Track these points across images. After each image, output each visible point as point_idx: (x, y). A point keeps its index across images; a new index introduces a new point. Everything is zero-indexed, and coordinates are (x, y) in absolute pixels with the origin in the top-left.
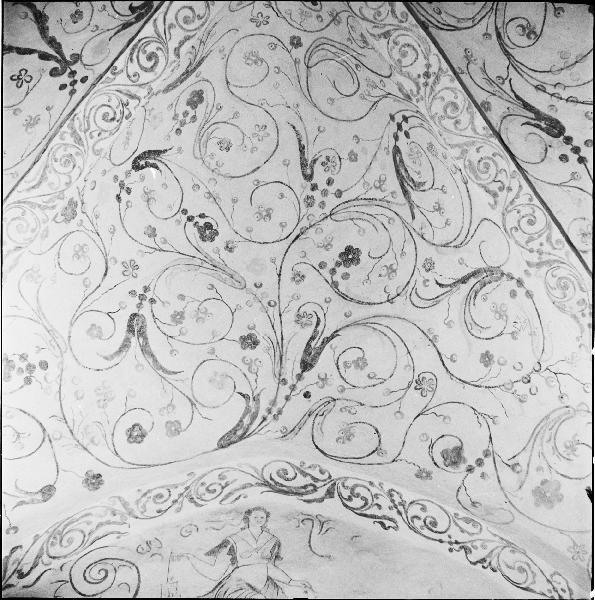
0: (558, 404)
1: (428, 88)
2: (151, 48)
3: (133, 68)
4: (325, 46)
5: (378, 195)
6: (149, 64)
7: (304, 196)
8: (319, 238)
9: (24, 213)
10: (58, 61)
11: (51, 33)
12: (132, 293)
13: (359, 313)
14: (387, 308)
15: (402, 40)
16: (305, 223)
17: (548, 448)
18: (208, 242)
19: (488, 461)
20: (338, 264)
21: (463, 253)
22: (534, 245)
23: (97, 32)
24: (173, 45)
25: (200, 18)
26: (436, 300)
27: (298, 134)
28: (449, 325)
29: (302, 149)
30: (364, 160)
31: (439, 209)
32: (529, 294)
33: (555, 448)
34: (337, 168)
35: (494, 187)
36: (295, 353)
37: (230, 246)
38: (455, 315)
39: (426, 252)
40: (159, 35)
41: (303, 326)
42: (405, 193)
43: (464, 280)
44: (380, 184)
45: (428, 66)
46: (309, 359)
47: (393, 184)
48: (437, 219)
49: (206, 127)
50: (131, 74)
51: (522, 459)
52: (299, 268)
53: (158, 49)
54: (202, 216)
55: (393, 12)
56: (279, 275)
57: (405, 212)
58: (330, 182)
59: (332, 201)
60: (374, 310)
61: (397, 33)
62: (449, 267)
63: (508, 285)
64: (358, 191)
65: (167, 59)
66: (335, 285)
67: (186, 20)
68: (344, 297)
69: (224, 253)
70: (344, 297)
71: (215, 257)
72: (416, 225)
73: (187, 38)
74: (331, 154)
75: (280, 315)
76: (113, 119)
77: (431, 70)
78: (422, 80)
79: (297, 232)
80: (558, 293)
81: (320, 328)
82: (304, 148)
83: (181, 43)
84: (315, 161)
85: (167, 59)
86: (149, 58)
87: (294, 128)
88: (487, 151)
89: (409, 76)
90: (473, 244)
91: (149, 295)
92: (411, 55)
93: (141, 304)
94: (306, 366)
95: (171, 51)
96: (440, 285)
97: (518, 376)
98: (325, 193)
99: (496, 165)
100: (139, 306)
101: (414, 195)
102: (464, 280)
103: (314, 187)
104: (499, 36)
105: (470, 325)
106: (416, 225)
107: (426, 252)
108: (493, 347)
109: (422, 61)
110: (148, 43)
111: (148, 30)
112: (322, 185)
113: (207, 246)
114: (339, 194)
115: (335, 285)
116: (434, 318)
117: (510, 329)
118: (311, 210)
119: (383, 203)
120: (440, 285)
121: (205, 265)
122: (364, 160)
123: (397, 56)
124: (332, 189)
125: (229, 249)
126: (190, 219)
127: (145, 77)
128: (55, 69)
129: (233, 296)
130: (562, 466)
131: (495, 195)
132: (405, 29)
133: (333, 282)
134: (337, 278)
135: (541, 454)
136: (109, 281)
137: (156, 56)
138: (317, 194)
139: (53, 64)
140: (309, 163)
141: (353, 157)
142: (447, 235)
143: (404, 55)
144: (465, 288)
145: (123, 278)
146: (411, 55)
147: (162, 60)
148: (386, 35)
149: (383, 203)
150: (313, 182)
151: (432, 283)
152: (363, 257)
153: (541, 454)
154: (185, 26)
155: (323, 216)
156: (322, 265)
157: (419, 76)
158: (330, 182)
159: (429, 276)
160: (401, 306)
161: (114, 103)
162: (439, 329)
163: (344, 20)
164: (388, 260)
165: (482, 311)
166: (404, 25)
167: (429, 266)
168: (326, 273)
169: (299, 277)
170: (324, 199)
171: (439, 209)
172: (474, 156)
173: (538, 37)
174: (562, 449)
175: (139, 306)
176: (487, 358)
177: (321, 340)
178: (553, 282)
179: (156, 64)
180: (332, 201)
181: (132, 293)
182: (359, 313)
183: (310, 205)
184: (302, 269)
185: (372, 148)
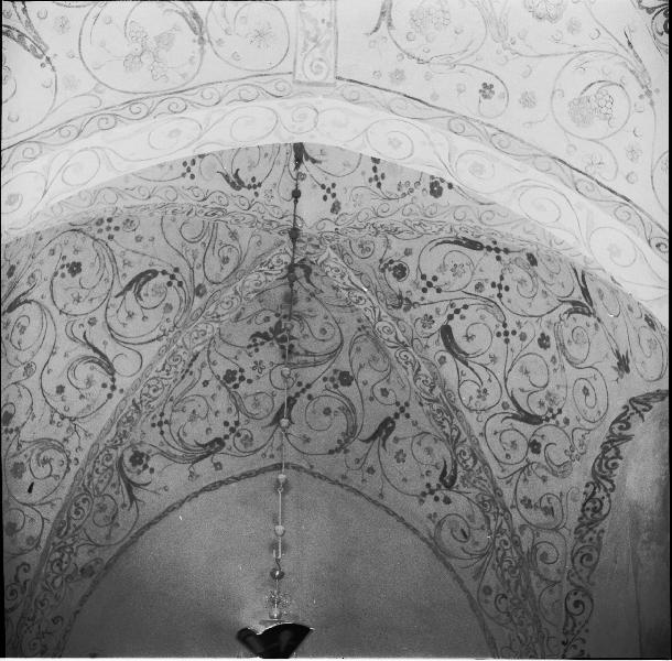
0: (61, 441)
5: (120, 264)
8: (79, 243)
13: (47, 302)
14: (55, 313)
15: (235, 301)
16: (85, 228)
17: (37, 451)
19: (14, 433)
21: (111, 342)
22: (144, 397)
26: (74, 339)
28: (66, 355)
30: (139, 247)
31: (131, 315)
32: (110, 396)
33: (39, 455)
35: (167, 367)
38: (73, 355)
39: (99, 316)
42: (129, 286)
43: (96, 350)
44: (127, 263)
47: (132, 273)
48: (123, 315)
51: (24, 446)
57: (117, 290)
59: (104, 236)
60: (52, 308)
62: (98, 336)
63: (107, 380)
64: (117, 250)
66: (56, 274)
72: (113, 301)
74: (136, 222)
79: (78, 228)
80: (125, 419)
88: (185, 357)
90: (120, 349)
96: (84, 336)
97: (61, 410)
101: (130, 294)
102: (96, 350)
105: (72, 368)
106: (113, 301)
107: (99, 316)
108: (69, 389)
112: (112, 225)
114: (111, 237)
115: (56, 274)
116: (65, 344)
117: (83, 392)
119: (116, 271)
120: (84, 336)
122: (139, 247)
123: (226, 300)
124: (112, 232)
130: (34, 464)
131: (163, 369)
135: (32, 451)
138: (106, 224)
141: (139, 239)
142: (117, 327)
143: (227, 303)
144: (90, 352)
148: (236, 293)
149: (116, 271)
151: (83, 329)
152: (78, 276)
153: (32, 451)
158: (117, 228)
159: (87, 326)
160: (61, 320)
162: (60, 353)
164: (83, 293)
165: (84, 371)
167: (92, 322)
171: (131, 315)
172: (181, 352)
174: (41, 458)
176: (60, 389)
178: (130, 415)
180: (104, 236)
182: (47, 302)
183: (97, 224)
185: (149, 251)
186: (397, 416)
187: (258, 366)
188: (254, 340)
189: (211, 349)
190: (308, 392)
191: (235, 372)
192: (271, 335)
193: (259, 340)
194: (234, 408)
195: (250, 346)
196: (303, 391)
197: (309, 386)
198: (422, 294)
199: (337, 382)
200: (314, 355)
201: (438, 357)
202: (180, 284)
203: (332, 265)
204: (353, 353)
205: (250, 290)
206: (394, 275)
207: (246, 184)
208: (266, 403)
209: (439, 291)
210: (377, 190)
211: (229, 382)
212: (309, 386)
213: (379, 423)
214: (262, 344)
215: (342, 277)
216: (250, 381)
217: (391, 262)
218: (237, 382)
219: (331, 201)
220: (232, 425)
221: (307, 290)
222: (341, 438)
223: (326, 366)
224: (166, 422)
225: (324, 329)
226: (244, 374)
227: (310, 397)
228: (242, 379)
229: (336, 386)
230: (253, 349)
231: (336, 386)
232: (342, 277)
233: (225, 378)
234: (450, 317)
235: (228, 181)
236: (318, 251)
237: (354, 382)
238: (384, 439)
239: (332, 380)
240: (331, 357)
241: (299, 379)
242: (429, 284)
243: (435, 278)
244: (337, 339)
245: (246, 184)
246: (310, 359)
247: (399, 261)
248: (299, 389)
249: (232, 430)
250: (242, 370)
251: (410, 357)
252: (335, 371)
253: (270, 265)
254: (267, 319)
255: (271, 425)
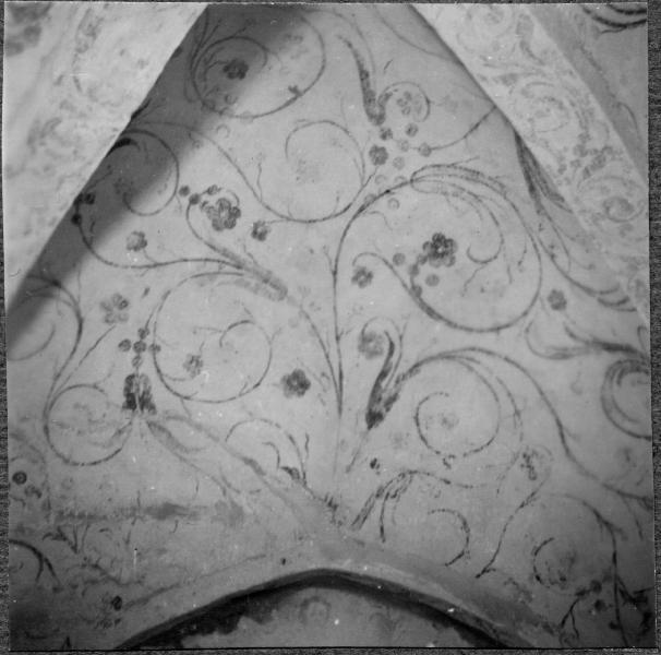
7: (369, 146)
12: (125, 345)
14: (488, 341)
16: (373, 189)
18: (226, 231)
20: (424, 260)
27: (356, 55)
29: (364, 75)
34: (424, 113)
36: (358, 399)
37: (259, 230)
41: (373, 354)
46: (379, 407)
49: (201, 52)
52: (362, 262)
54: (209, 191)
56: (335, 273)
58: (411, 131)
59: (414, 162)
61: (530, 79)
68: (430, 312)
69: (254, 246)
70: (430, 312)
71: (238, 251)
74: (414, 91)
75: (338, 338)
77: (589, 146)
81: (394, 359)
82: (367, 75)
84: (388, 96)
91: (148, 340)
93: (138, 358)
94: (374, 418)
98: (404, 147)
100: (137, 362)
103: (385, 135)
112: (399, 130)
113: (226, 239)
115: (416, 292)
118: (382, 169)
121: (227, 268)
124: (416, 141)
125: (259, 234)
126: (194, 200)
129: (267, 311)
133: (414, 287)
134: (420, 280)
136: (88, 338)
140: (377, 97)
145: (106, 327)
150: (385, 125)
152: (460, 254)
155: (400, 181)
156: (398, 259)
158: (411, 131)
168: (403, 270)
169: (363, 277)
170: (404, 155)
175: (137, 362)
177: (394, 379)
181: (125, 345)
184: (367, 263)
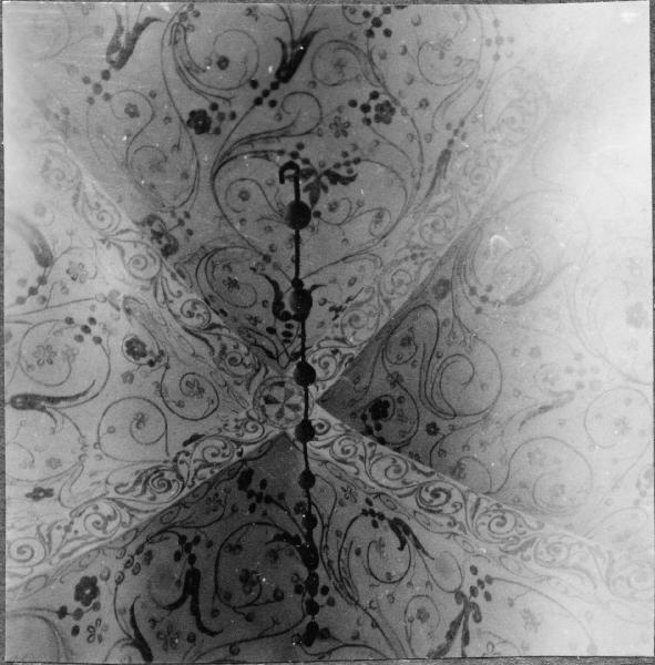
1: (426, 251)
2: (427, 497)
3: (448, 509)
4: (428, 394)
6: (443, 496)
9: (621, 578)
10: (467, 620)
11: (443, 641)
15: (389, 287)
23: (432, 581)
24: (422, 479)
25: (395, 461)
40: (414, 491)
45: (406, 259)
50: (454, 509)
53: (427, 490)
55: (367, 301)
58: (569, 371)
61: (383, 291)
65: (436, 481)
67: (398, 471)
73: (415, 468)
76: (503, 518)
78: (420, 259)
83: (420, 472)
85: (436, 481)
86: (437, 496)
87: (523, 422)
89: (418, 272)
92: (401, 276)
95: (429, 479)
99: (474, 169)
103: (580, 386)
104: (384, 237)
109: (404, 265)
110: (422, 500)
111: (243, 50)
127: (456, 497)
128: (474, 617)
132: (379, 288)
137: (436, 490)
139: (472, 625)
143: (401, 282)
146: (401, 276)
147: (438, 485)
148: (387, 301)
154: (403, 472)
157: (416, 264)
161: (486, 520)
163: (396, 368)
166: (376, 289)
173: (381, 209)
179: (441, 490)
186: (106, 75)
187: (341, 129)
188: (350, 171)
189: (417, 164)
190: (258, 93)
191: (378, 119)
192: (325, 180)
193: (343, 172)
194: (376, 58)
195: (357, 161)
196: (266, 93)
197: (258, 102)
198: (95, 315)
199: (213, 115)
200: (255, 154)
201: (48, 216)
202: (448, 126)
203: (241, 371)
204: (193, 167)
205: (366, 308)
206: (144, 346)
207: (385, 523)
208: (324, 68)
209: (70, 321)
210: (182, 532)
211: (388, 103)
212: (258, 102)
213: (134, 54)
214: (338, 166)
215: (224, 348)
216: (353, 104)
217: (151, 363)
218: (373, 104)
219: (255, 486)
220: (378, 32)
221: (276, 267)
222: (194, 21)
223: (235, 137)
224: (489, 42)
225: (244, 199)
226: (362, 115)
227: (254, 84)
228: (366, 108)
229: (214, 107)
230: (352, 156)
231: (214, 107)
232: (224, 348)
233: (392, 111)
234: (42, 280)
235: (415, 538)
236: (266, 393)
237: (186, 118)
238: (120, 30)
239: (221, 117)
240: (228, 154)
241: (273, 112)
242: (86, 329)
243: (79, 339)
244: (221, 183)
245: (385, 523)
246: (259, 146)
247: (141, 365)
248: (273, 95)
249: (377, 23)
250: (368, 121)
251: (93, 218)
252: (218, 131)
253: (338, 356)
254: (333, 207)
255: (314, 34)
